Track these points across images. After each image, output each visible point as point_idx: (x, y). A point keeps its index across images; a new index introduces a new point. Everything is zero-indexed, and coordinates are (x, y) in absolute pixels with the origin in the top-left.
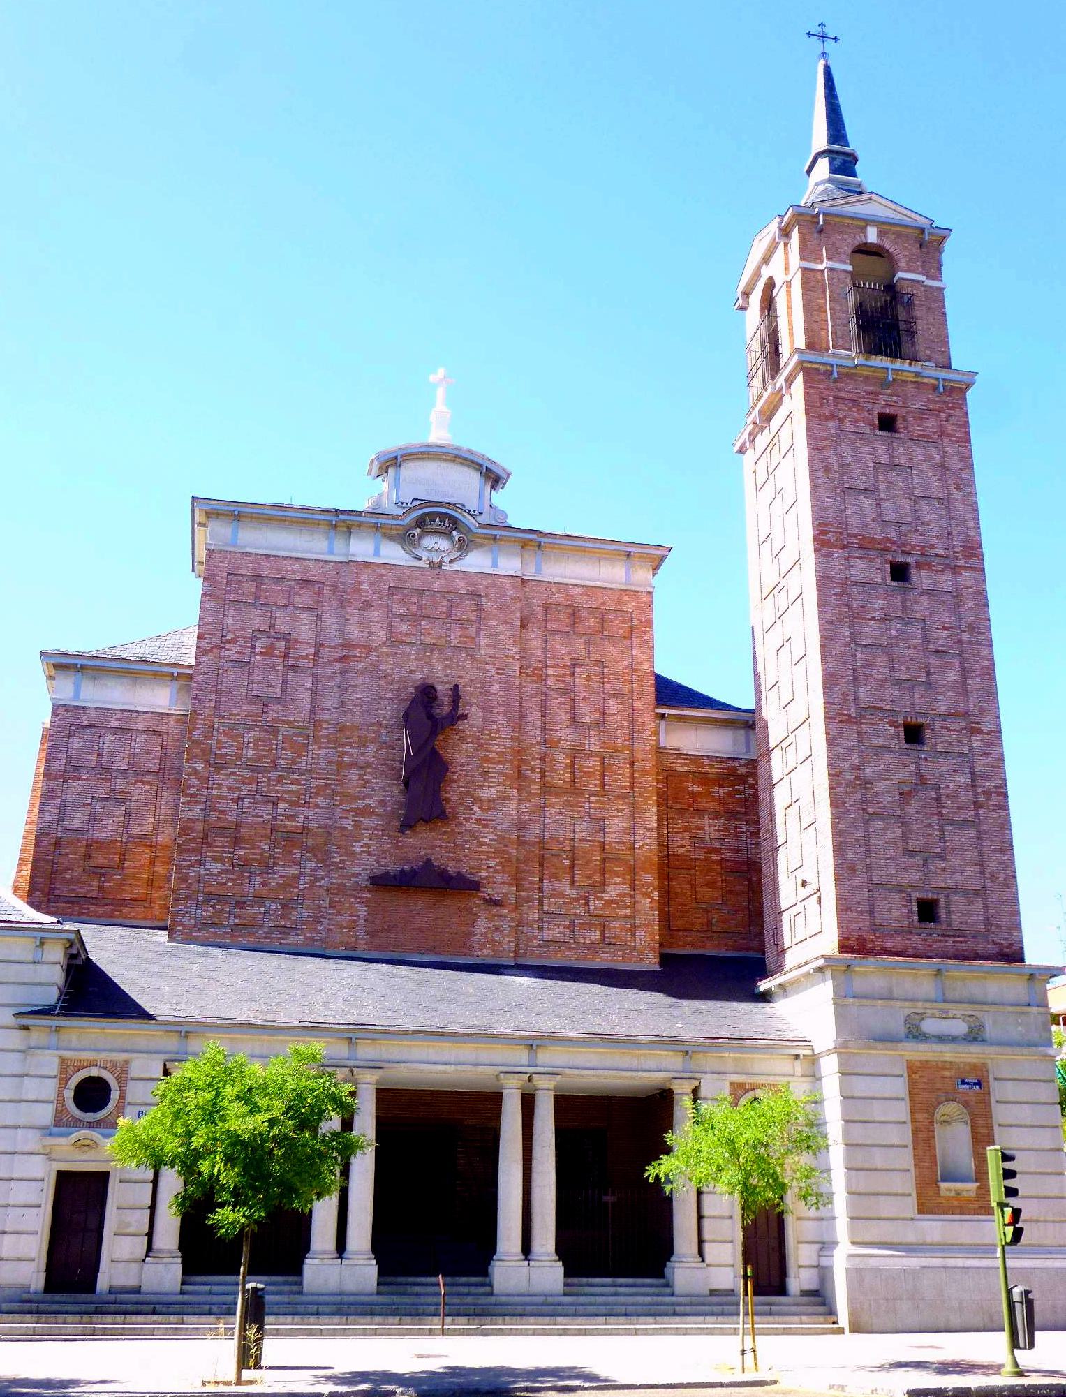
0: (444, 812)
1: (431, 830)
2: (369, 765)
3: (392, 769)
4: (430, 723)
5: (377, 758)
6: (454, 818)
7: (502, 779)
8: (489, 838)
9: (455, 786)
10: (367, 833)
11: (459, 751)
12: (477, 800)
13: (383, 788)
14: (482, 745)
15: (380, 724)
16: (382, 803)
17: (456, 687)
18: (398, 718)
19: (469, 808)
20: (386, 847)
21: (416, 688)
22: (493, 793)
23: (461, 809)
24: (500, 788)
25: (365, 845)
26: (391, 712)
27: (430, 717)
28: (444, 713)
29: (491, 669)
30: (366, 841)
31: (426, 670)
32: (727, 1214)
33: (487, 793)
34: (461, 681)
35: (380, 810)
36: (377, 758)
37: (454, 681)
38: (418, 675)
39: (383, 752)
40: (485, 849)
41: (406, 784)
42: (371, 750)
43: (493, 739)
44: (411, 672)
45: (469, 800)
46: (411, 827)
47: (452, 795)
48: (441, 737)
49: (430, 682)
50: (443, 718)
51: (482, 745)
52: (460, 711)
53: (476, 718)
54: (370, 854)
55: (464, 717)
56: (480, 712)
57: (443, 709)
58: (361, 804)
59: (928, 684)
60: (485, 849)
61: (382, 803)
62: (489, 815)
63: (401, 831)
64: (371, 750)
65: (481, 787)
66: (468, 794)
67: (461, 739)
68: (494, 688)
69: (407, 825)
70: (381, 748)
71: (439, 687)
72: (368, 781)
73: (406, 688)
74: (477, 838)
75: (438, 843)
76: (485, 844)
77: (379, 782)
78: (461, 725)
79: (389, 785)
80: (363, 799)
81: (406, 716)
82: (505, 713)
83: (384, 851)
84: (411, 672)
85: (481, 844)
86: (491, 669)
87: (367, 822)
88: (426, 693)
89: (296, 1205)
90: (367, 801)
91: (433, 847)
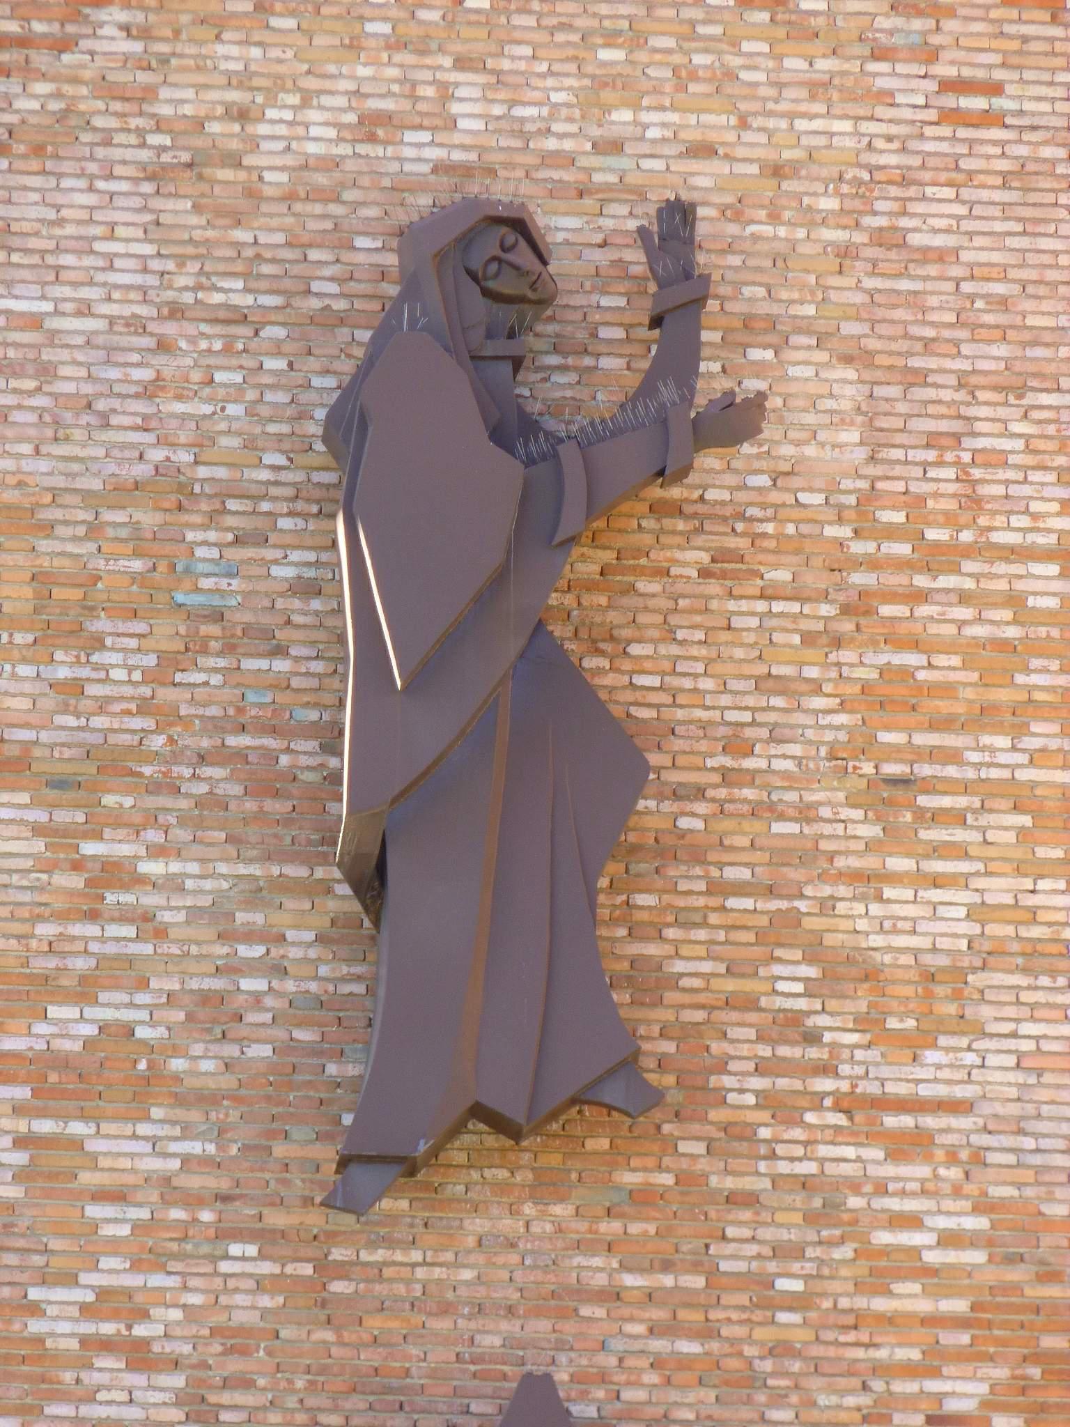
0: (629, 1063)
1: (547, 1187)
2: (112, 763)
3: (265, 782)
4: (506, 471)
5: (167, 718)
6: (700, 1091)
7: (1006, 825)
8: (937, 1223)
9: (691, 879)
10: (115, 1223)
11: (709, 652)
12: (844, 971)
13: (217, 918)
14: (859, 607)
15: (175, 491)
16: (214, 1015)
17: (679, 215)
18: (296, 447)
19: (793, 1027)
20: (246, 1308)
21: (407, 237)
22: (946, 923)
23: (741, 1040)
24: (999, 890)
25: (108, 1302)
26: (250, 407)
27: (512, 429)
28: (605, 400)
29: (910, 88)
30: (113, 1272)
31: (470, 112)
32: (353, 1169)
33: (918, 922)
34: (702, 180)
35: (201, 1063)
36: (167, 718)
37: (664, 174)
38: (418, 151)
39: (206, 674)
40: (909, 1297)
41: (371, 881)
42: (121, 664)
43: (939, 559)
44: (372, 126)
45: (790, 981)
46: (411, 1168)
47: (676, 949)
48: (586, 563)
49: (502, 192)
50: (587, 442)
51: (859, 607)
52: (712, 379)
53: (816, 421)
54: (140, 1356)
55: (736, 421)
56: (846, 386)
57: (590, 369)
58: (68, 1026)
59: (983, 1066)
60: (909, 1297)
61: (214, 1015)
62: (935, 1071)
63: (345, 1201)
64: (121, 664)
65: (870, 882)
66: (780, 932)
67: (724, 567)
68: (933, 219)
69: (380, 1160)
70: (194, 648)
71: (559, 225)
72: (115, 873)
73: (341, 240)
74: (853, 1228)
75: (596, 1268)
76: (910, 1265)
77: (188, 877)
78: (715, 475)
79: (256, 895)
80: (85, 991)
81: (349, 427)
82: (1014, 386)
83: (237, 1341)
84: (372, 126)
85: (883, 1270)
86: (910, 88)
87: (126, 1147)
88: (482, 268)
89: (590, 663)
90: (112, 1008)
91: (562, 1301)
